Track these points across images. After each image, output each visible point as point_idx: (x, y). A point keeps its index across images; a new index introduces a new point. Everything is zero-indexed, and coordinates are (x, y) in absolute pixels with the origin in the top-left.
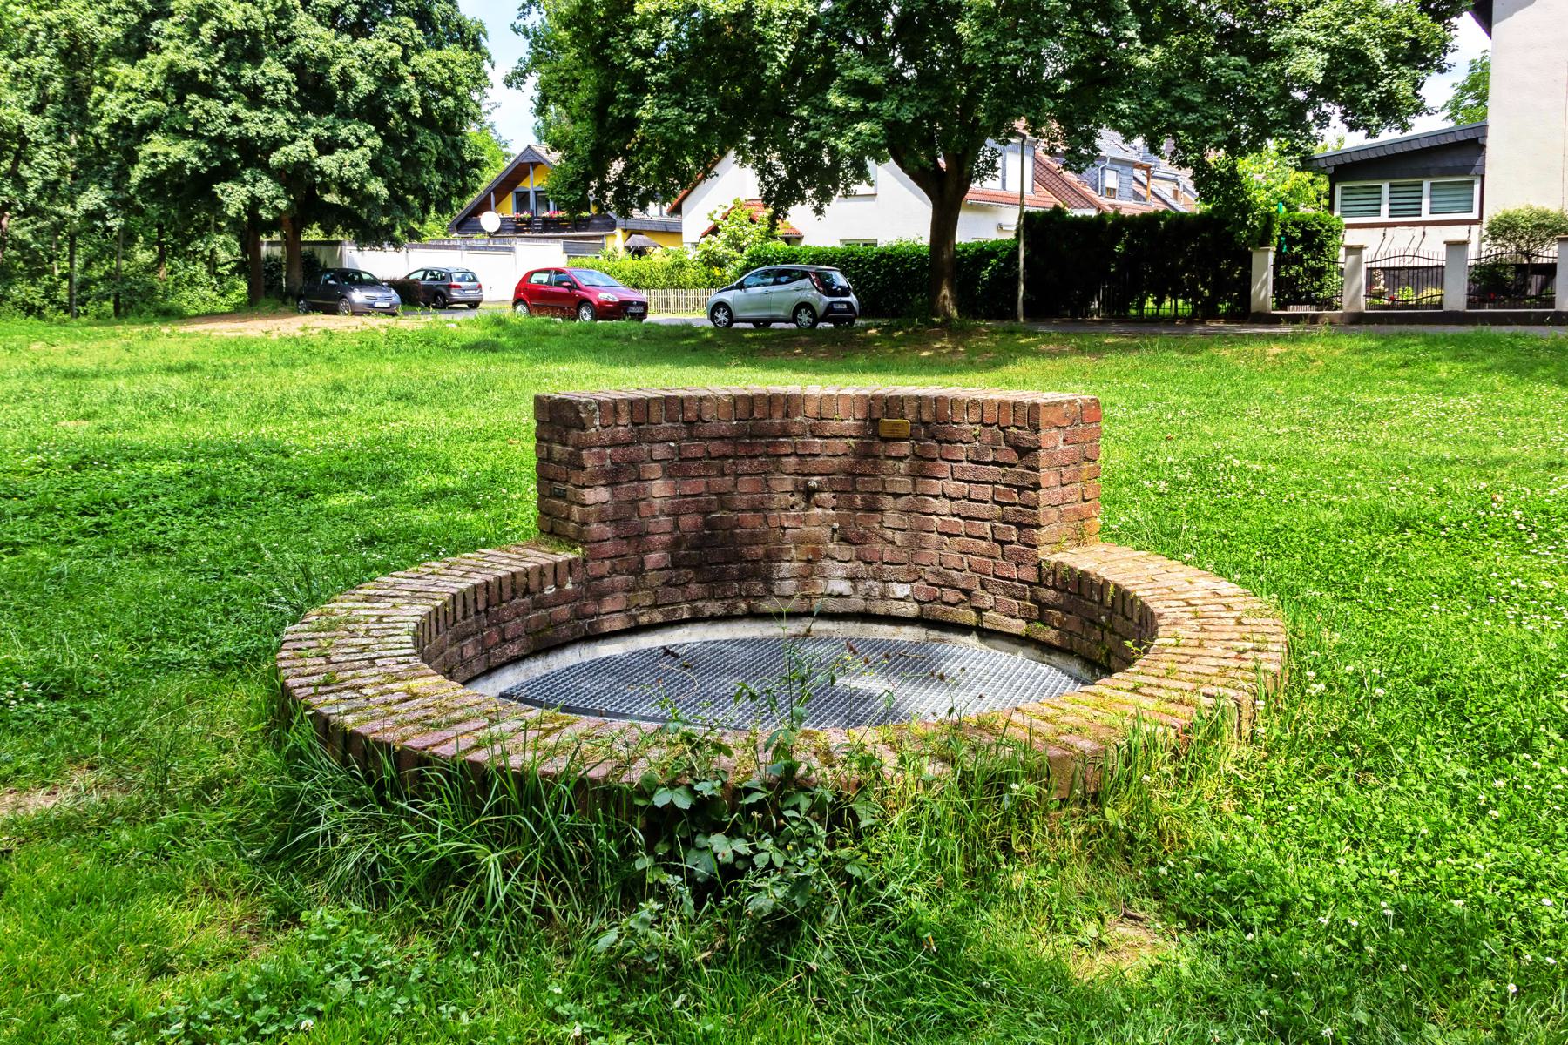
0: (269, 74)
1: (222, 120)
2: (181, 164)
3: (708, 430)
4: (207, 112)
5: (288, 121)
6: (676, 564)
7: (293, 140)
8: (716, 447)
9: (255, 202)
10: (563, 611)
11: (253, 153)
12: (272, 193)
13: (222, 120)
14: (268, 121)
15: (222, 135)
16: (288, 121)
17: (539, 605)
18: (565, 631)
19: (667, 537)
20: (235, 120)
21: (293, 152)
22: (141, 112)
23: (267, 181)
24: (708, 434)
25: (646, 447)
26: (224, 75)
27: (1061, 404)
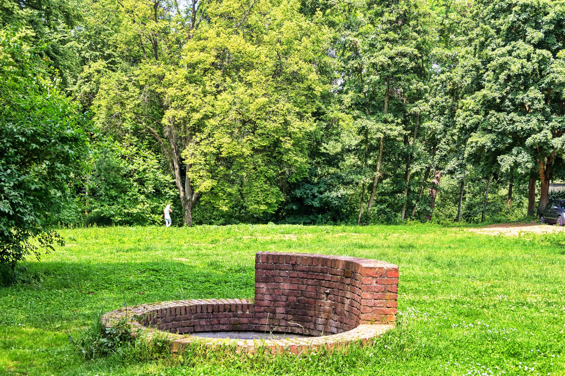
0: (530, 96)
1: (505, 123)
2: (483, 146)
3: (298, 268)
4: (498, 119)
5: (538, 120)
6: (287, 313)
7: (541, 130)
8: (301, 274)
9: (517, 164)
10: (245, 320)
11: (519, 139)
12: (525, 160)
13: (505, 123)
14: (529, 121)
15: (505, 130)
16: (538, 120)
17: (235, 316)
18: (244, 327)
19: (284, 303)
20: (512, 121)
21: (539, 137)
22: (471, 121)
23: (524, 153)
24: (298, 269)
25: (278, 271)
26: (509, 99)
27: (375, 268)
